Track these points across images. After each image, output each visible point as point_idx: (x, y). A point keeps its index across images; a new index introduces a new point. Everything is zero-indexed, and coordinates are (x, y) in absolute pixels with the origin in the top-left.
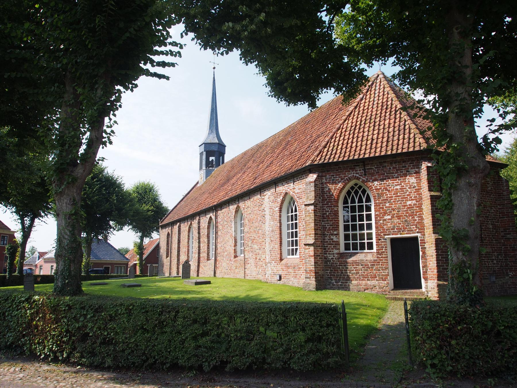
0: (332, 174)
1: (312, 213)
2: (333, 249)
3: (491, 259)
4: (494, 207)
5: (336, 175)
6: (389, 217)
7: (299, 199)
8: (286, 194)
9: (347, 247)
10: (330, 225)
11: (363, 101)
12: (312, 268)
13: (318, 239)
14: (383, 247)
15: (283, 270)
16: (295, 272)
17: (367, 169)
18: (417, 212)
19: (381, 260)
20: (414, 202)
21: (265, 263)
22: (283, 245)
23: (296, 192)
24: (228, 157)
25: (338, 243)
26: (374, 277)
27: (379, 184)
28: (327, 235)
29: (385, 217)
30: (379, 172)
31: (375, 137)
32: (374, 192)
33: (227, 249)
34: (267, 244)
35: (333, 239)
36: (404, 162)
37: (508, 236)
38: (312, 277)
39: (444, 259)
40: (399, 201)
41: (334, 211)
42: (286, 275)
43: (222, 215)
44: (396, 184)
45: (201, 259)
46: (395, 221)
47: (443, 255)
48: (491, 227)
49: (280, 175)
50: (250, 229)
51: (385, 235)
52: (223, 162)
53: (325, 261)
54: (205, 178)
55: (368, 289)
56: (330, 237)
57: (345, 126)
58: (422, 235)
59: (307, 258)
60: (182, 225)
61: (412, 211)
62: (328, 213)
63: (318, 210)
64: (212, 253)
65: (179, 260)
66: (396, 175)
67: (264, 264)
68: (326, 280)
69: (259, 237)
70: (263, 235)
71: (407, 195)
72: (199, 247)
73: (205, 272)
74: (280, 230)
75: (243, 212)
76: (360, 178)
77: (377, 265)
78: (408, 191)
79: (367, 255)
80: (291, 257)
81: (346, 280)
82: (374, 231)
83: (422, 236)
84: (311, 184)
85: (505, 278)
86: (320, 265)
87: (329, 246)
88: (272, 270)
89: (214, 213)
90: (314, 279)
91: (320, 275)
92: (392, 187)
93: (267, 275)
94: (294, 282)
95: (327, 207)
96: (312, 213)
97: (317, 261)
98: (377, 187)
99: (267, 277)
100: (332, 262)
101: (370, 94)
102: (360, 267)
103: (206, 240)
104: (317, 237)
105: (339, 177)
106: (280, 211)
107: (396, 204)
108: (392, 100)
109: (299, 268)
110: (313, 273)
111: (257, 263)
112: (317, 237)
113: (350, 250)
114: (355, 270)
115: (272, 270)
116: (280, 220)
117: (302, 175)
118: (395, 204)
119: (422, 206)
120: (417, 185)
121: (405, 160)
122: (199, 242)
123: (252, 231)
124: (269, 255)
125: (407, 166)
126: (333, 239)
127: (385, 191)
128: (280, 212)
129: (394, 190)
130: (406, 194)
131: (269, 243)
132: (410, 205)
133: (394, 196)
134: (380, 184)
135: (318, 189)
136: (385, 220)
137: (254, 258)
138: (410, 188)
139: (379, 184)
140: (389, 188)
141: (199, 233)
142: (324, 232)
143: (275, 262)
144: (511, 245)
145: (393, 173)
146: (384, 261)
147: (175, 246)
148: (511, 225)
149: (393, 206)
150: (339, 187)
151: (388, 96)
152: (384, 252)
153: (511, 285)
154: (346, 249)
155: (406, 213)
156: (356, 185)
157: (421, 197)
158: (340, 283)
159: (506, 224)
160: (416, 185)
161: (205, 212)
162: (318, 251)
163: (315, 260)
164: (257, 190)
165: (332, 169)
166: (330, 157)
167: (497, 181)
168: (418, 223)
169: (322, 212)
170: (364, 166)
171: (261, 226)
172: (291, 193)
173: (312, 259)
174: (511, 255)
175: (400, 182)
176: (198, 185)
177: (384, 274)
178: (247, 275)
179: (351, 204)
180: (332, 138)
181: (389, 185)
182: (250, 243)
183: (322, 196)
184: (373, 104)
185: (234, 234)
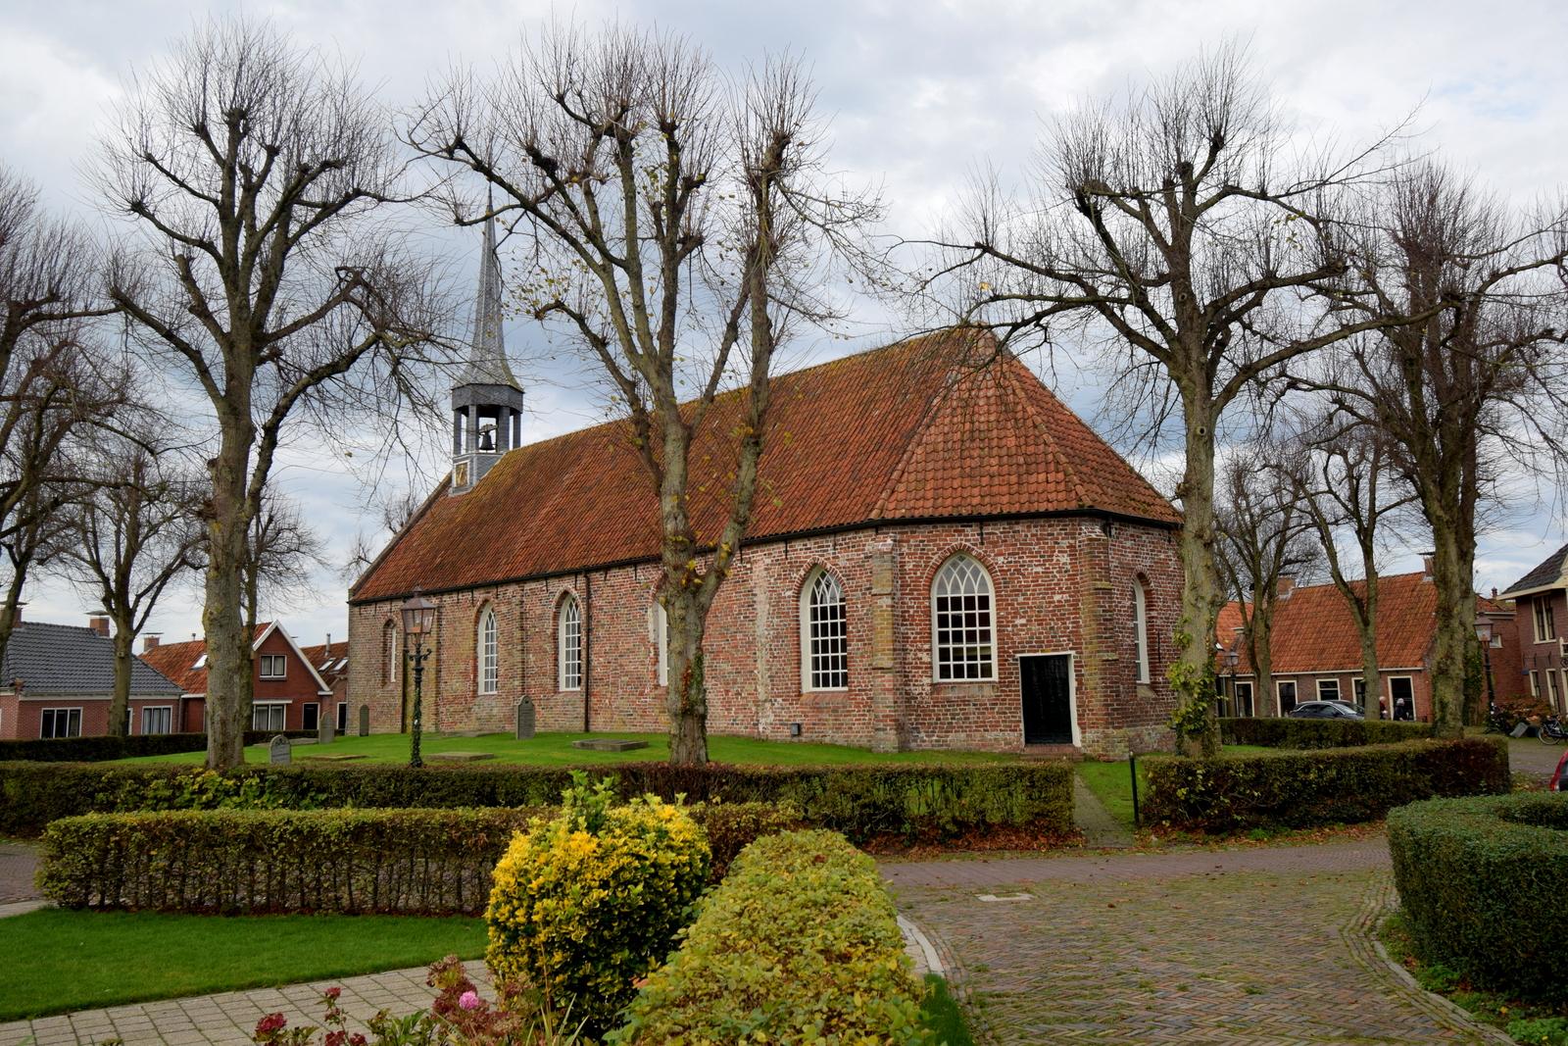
6: (1023, 621)
9: (944, 672)
20: (1066, 596)
26: (995, 726)
34: (761, 665)
80: (821, 689)
82: (994, 644)
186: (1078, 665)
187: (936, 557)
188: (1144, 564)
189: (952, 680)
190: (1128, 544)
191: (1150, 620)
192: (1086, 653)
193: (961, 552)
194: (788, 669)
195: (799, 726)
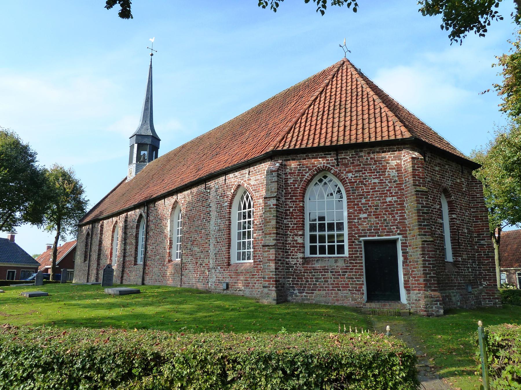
3: (467, 267)
4: (468, 210)
6: (365, 215)
7: (255, 192)
8: (239, 186)
9: (313, 250)
10: (295, 224)
11: (330, 87)
12: (272, 275)
13: (279, 240)
14: (357, 251)
16: (246, 280)
20: (395, 198)
21: (208, 269)
22: (232, 247)
24: (161, 152)
26: (346, 287)
27: (353, 176)
28: (290, 235)
31: (348, 123)
32: (348, 186)
34: (212, 246)
35: (297, 241)
37: (482, 242)
38: (271, 286)
39: (431, 266)
41: (299, 207)
44: (374, 177)
46: (372, 220)
47: (430, 261)
48: (466, 231)
49: (231, 164)
51: (360, 236)
52: (156, 157)
53: (287, 267)
56: (293, 238)
57: (310, 111)
58: (403, 237)
59: (267, 263)
63: (280, 205)
64: (140, 256)
66: (374, 166)
69: (201, 237)
70: (206, 235)
71: (387, 190)
76: (332, 169)
77: (350, 272)
81: (312, 290)
82: (346, 232)
85: (478, 287)
86: (281, 272)
91: (280, 284)
92: (370, 180)
93: (210, 284)
95: (290, 202)
97: (278, 266)
98: (351, 180)
99: (210, 285)
100: (295, 268)
101: (337, 81)
103: (134, 242)
104: (279, 237)
108: (362, 87)
109: (253, 275)
110: (273, 281)
111: (197, 269)
112: (279, 237)
115: (217, 277)
118: (372, 200)
124: (213, 259)
126: (297, 241)
129: (371, 184)
131: (214, 245)
132: (390, 202)
133: (371, 191)
134: (355, 177)
135: (281, 180)
136: (360, 219)
137: (194, 263)
138: (389, 182)
139: (353, 176)
140: (366, 181)
142: (287, 232)
143: (221, 268)
145: (370, 165)
148: (485, 230)
149: (370, 203)
150: (306, 179)
151: (357, 83)
152: (358, 257)
153: (485, 296)
154: (239, 259)
155: (386, 211)
158: (305, 294)
160: (397, 179)
162: (279, 254)
163: (276, 266)
166: (296, 143)
167: (470, 182)
168: (399, 223)
170: (337, 155)
171: (204, 225)
172: (245, 185)
173: (273, 265)
175: (379, 175)
176: (126, 181)
177: (358, 282)
178: (185, 283)
180: (296, 123)
183: (285, 189)
184: (341, 91)
186: (404, 245)
187: (307, 175)
188: (448, 183)
189: (318, 255)
190: (437, 168)
191: (452, 220)
193: (323, 171)
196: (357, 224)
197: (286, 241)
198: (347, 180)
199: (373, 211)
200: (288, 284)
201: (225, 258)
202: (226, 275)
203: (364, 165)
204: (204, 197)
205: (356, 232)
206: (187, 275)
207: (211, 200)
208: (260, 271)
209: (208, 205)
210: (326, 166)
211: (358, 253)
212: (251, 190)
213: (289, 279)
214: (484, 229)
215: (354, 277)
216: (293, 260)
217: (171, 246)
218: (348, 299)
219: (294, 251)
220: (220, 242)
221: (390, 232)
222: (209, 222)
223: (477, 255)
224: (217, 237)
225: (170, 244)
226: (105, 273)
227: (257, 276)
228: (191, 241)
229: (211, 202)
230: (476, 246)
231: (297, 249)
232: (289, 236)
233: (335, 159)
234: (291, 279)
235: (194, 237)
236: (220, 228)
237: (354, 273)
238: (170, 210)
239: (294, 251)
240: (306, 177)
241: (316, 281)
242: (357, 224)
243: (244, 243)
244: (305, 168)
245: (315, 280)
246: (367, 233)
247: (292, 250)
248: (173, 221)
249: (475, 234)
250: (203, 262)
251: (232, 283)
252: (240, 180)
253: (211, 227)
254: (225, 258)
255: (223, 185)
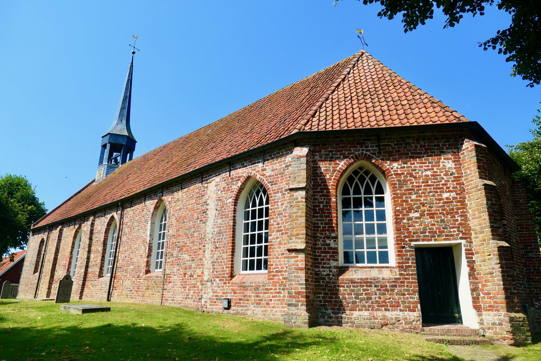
0: (330, 149)
1: (302, 202)
2: (329, 260)
5: (336, 151)
6: (417, 215)
7: (272, 185)
8: (249, 177)
10: (326, 224)
12: (302, 288)
15: (235, 293)
16: (257, 296)
17: (383, 145)
18: (459, 209)
19: (406, 279)
20: (453, 194)
23: (267, 175)
24: (138, 154)
25: (335, 251)
26: (395, 306)
27: (399, 167)
28: (321, 238)
29: (411, 215)
30: (399, 151)
32: (393, 178)
33: (135, 260)
34: (208, 254)
35: (329, 244)
36: (436, 139)
38: (300, 303)
40: (431, 192)
42: (240, 300)
43: (131, 212)
44: (426, 168)
45: (89, 275)
46: (426, 220)
50: (178, 230)
51: (411, 241)
52: (131, 158)
53: (316, 278)
54: (105, 175)
55: (387, 325)
56: (324, 241)
58: (467, 242)
60: (65, 229)
61: (451, 207)
62: (322, 205)
64: (107, 266)
65: (53, 277)
67: (199, 284)
68: (317, 309)
69: (193, 242)
71: (443, 185)
72: (88, 258)
73: (94, 294)
74: (234, 232)
75: (168, 207)
77: (400, 286)
78: (443, 179)
79: (381, 271)
80: (248, 272)
82: (390, 235)
83: (469, 244)
84: (301, 159)
87: (323, 255)
88: (214, 292)
89: (119, 212)
90: (304, 308)
92: (420, 172)
93: (203, 300)
94: (255, 312)
95: (320, 196)
96: (302, 202)
98: (397, 171)
102: (374, 289)
103: (100, 249)
105: (341, 154)
106: (235, 204)
107: (426, 196)
110: (302, 297)
111: (186, 282)
113: (364, 263)
114: (366, 294)
115: (214, 292)
116: (234, 217)
117: (280, 149)
119: (465, 201)
120: (457, 171)
121: (437, 136)
122: (89, 252)
123: (182, 234)
125: (441, 144)
126: (329, 244)
127: (409, 178)
128: (235, 205)
130: (441, 183)
131: (212, 251)
132: (447, 198)
133: (423, 184)
134: (401, 168)
137: (181, 275)
138: (446, 175)
139: (399, 167)
141: (91, 239)
142: (316, 234)
144: (535, 266)
146: (410, 280)
147: (49, 257)
148: (532, 241)
149: (422, 199)
150: (340, 168)
155: (442, 210)
156: (361, 168)
157: (463, 188)
159: (526, 240)
160: (454, 171)
161: (105, 210)
164: (196, 175)
165: (329, 142)
168: (460, 224)
169: (313, 203)
170: (379, 141)
174: (535, 279)
175: (432, 166)
176: (94, 184)
177: (411, 300)
178: (166, 300)
179: (354, 194)
181: (416, 170)
182: (175, 253)
183: (313, 180)
185: (148, 239)
186: (470, 253)
192: (475, 242)
194: (225, 256)
195: (229, 302)
196: (406, 225)
197: (315, 245)
198: (392, 171)
199: (426, 209)
200: (319, 301)
201: (226, 267)
202: (227, 289)
203: (412, 153)
204: (199, 192)
205: (406, 234)
206: (170, 289)
207: (209, 196)
208: (278, 284)
209: (204, 202)
210: (366, 154)
211: (410, 262)
212: (266, 182)
213: (319, 295)
214: (531, 239)
215: (406, 293)
216: (325, 269)
217: (150, 253)
218: (400, 322)
219: (325, 258)
220: (220, 248)
221: (449, 236)
222: (204, 223)
223: (525, 270)
224: (216, 240)
225: (148, 251)
226: (61, 285)
227: (273, 291)
228: (179, 247)
229: (208, 199)
230: (523, 259)
231: (330, 256)
232: (318, 238)
233: (376, 146)
234: (323, 295)
235: (183, 242)
236: (220, 230)
237: (406, 288)
238: (151, 210)
239: (325, 258)
240: (340, 166)
241: (355, 298)
242: (406, 225)
243: (252, 249)
244: (339, 156)
245: (354, 296)
246: (421, 236)
247: (323, 256)
248: (154, 223)
249: (521, 246)
250: (194, 273)
251: (235, 300)
252: (251, 171)
253: (207, 229)
254: (226, 267)
255: (227, 177)
